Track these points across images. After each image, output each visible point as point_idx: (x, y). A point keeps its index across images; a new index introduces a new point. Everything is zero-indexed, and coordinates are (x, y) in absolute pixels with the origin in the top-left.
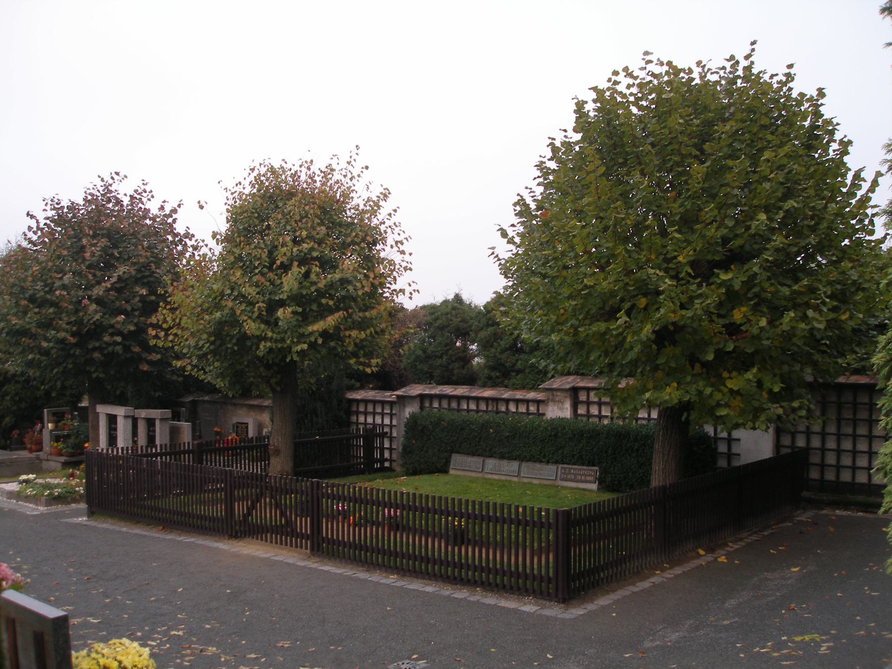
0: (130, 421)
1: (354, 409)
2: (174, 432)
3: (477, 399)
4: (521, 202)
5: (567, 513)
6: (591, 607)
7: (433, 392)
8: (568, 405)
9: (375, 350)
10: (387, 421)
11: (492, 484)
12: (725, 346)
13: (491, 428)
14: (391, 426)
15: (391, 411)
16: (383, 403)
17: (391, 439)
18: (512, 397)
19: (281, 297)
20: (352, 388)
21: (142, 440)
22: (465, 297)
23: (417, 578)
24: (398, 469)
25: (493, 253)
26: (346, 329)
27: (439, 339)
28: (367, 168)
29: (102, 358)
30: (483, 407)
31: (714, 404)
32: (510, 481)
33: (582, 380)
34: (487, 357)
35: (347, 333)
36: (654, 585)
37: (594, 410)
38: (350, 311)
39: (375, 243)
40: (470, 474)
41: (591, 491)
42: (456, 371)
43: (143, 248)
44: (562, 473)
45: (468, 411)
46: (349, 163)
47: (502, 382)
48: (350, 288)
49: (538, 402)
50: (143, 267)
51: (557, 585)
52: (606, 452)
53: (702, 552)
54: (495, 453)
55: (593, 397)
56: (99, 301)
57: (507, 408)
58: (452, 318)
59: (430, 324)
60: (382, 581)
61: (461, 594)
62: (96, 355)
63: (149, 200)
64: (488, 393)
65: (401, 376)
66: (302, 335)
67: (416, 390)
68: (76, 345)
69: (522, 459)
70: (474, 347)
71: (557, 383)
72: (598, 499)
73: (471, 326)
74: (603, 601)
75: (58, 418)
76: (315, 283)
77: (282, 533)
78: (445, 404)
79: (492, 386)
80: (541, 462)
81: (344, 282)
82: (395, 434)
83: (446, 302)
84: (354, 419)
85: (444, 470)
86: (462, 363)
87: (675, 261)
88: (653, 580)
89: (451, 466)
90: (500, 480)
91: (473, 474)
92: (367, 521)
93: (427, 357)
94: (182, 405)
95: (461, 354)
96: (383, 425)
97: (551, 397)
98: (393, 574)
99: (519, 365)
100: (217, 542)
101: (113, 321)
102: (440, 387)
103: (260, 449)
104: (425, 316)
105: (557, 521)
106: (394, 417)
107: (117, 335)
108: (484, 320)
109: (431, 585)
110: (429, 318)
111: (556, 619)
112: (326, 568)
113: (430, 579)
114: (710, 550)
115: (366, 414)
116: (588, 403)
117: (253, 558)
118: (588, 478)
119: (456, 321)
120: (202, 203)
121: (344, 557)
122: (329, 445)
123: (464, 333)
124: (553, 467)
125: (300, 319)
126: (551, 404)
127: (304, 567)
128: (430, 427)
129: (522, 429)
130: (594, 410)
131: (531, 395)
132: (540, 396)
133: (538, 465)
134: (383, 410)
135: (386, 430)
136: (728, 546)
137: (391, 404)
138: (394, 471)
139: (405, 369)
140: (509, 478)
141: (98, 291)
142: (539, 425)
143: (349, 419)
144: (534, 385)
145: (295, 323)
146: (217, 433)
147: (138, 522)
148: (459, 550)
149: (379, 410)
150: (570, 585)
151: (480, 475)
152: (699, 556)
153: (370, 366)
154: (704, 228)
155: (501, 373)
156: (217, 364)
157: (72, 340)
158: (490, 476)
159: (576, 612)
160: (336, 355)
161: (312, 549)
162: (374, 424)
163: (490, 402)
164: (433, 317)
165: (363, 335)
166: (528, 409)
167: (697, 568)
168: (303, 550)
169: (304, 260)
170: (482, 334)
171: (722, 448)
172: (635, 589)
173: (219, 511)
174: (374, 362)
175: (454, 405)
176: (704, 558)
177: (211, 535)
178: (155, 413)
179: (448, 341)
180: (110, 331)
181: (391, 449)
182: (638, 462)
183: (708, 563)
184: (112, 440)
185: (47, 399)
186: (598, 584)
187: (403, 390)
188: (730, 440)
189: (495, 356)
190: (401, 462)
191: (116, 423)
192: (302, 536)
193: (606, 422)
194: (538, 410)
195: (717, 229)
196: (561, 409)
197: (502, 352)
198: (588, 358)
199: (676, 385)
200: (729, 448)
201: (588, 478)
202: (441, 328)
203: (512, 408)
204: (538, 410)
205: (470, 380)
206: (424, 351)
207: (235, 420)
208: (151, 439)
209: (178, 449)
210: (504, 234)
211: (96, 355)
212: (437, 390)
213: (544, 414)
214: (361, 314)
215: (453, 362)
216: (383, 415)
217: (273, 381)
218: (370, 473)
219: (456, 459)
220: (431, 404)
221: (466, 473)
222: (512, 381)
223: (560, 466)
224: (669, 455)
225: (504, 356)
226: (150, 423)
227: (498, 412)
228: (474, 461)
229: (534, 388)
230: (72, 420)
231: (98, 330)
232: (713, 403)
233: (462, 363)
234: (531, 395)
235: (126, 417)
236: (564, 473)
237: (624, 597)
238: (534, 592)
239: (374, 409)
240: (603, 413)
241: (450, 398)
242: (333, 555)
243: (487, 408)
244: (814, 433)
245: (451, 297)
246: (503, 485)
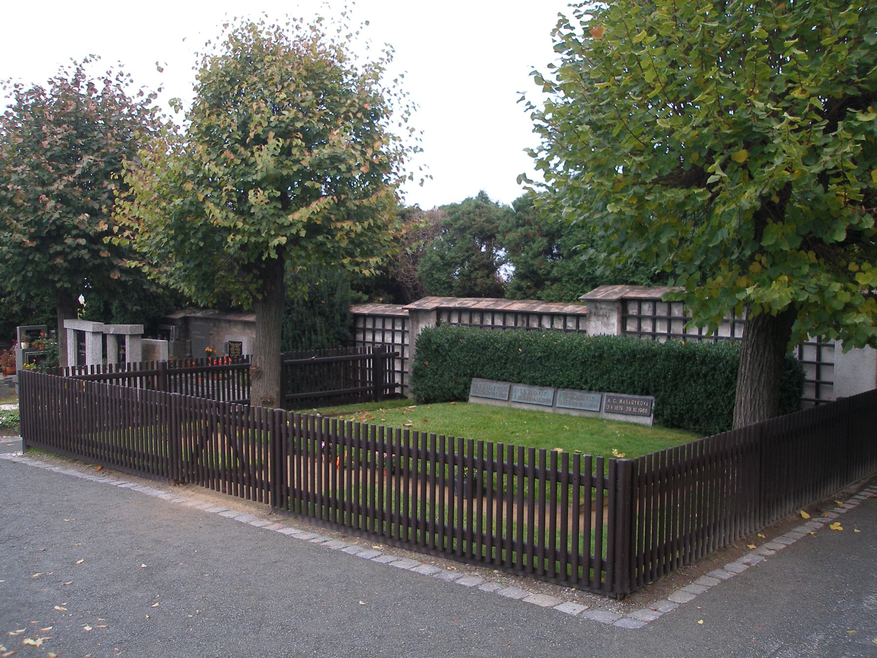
0: (100, 338)
1: (361, 325)
2: (148, 351)
3: (505, 313)
4: (563, 22)
5: (632, 466)
6: (664, 607)
7: (451, 305)
8: (614, 320)
9: (376, 248)
10: (398, 340)
11: (519, 416)
12: (861, 221)
13: (520, 346)
14: (403, 346)
15: (403, 328)
16: (394, 318)
17: (403, 361)
18: (545, 311)
19: (255, 177)
20: (358, 302)
21: (112, 359)
22: (493, 198)
23: (410, 549)
24: (410, 396)
25: (523, 98)
26: (338, 220)
27: (459, 243)
28: (367, 23)
29: (66, 265)
30: (511, 322)
31: (840, 307)
32: (543, 412)
33: (632, 290)
34: (516, 263)
35: (339, 225)
36: (751, 569)
37: (647, 327)
38: (343, 197)
39: (377, 117)
40: (493, 403)
41: (644, 426)
42: (479, 281)
43: (113, 136)
44: (607, 403)
45: (493, 327)
46: (343, 14)
47: (534, 294)
48: (343, 167)
49: (578, 317)
50: (115, 159)
51: (614, 572)
52: (664, 378)
53: (805, 515)
54: (525, 377)
55: (647, 310)
56: (62, 198)
57: (540, 324)
58: (475, 223)
59: (448, 226)
60: (361, 555)
61: (471, 579)
62: (59, 261)
63: (127, 85)
64: (517, 306)
65: (415, 288)
66: (282, 227)
67: (431, 303)
68: (37, 249)
69: (557, 385)
70: (502, 253)
71: (601, 293)
72: (676, 445)
73: (497, 227)
74: (682, 596)
75: (33, 335)
76: (297, 162)
77: (236, 479)
78: (465, 319)
79: (523, 299)
80: (582, 389)
81: (335, 159)
82: (407, 355)
83: (468, 200)
84: (360, 337)
85: (462, 398)
86: (486, 272)
87: (787, 97)
88: (746, 559)
89: (471, 393)
90: (531, 411)
91: (498, 403)
92: (359, 464)
93: (445, 265)
94: (172, 322)
95: (485, 261)
96: (393, 344)
97: (593, 310)
98: (378, 542)
99: (555, 273)
100: (159, 488)
101: (76, 222)
102: (461, 300)
103: (239, 367)
104: (444, 216)
105: (616, 478)
106: (406, 335)
107: (82, 237)
108: (513, 220)
109: (428, 563)
110: (448, 219)
111: (612, 629)
112: (288, 531)
113: (428, 554)
114: (816, 512)
115: (374, 331)
116: (640, 318)
117: (197, 514)
118: (641, 410)
119: (480, 221)
120: (162, 65)
121: (314, 516)
122: (327, 364)
123: (488, 237)
124: (596, 396)
125: (280, 206)
126: (593, 318)
127: (260, 529)
128: (447, 345)
129: (558, 348)
130: (647, 327)
131: (570, 308)
132: (580, 309)
133: (577, 393)
134: (393, 327)
135: (398, 350)
136: (837, 506)
137: (403, 319)
138: (406, 398)
139: (420, 279)
140: (541, 409)
141: (58, 186)
142: (580, 344)
143: (355, 337)
144: (572, 297)
145: (272, 211)
146: (209, 354)
147: (75, 460)
148: (468, 513)
149: (389, 327)
150: (630, 570)
152: (801, 521)
153: (367, 265)
154: (837, 43)
155: (532, 283)
156: (179, 264)
157: (29, 243)
158: (518, 406)
159: (642, 616)
160: (326, 253)
161: (274, 504)
162: (383, 343)
163: (519, 317)
164: (453, 217)
165: (359, 228)
166: (565, 325)
167: (803, 539)
168: (263, 504)
169: (285, 133)
170: (510, 236)
171: (810, 375)
172: (726, 576)
173: (164, 449)
174: (373, 261)
175: (476, 320)
176: (811, 526)
177: (155, 480)
178: (125, 329)
179: (470, 245)
180: (74, 232)
181: (402, 373)
182: (705, 390)
183: (818, 531)
184: (81, 359)
185: (26, 314)
186: (672, 568)
187: (417, 303)
188: (819, 365)
189: (526, 262)
190: (412, 388)
191: (84, 341)
192: (261, 485)
193: (663, 341)
194: (578, 326)
195: (850, 50)
196: (606, 325)
197: (535, 256)
198: (656, 242)
199: (786, 278)
200: (818, 375)
201: (641, 410)
202: (463, 230)
203: (546, 324)
204: (578, 326)
205: (497, 291)
206: (442, 258)
207: (228, 338)
208: (121, 358)
209: (150, 369)
210: (539, 80)
211: (59, 261)
212: (457, 303)
213: (585, 332)
214: (357, 202)
215: (476, 269)
216: (393, 332)
217: (253, 287)
218: (376, 401)
219: (478, 385)
220: (449, 320)
221: (489, 402)
222: (546, 292)
223: (606, 394)
224: (759, 380)
225: (536, 262)
226: (120, 340)
227: (528, 329)
228: (499, 388)
229: (573, 300)
230: (47, 339)
231: (59, 232)
232: (838, 305)
233: (486, 272)
234: (570, 308)
235: (94, 333)
237: (711, 589)
238: (578, 580)
239: (384, 325)
240: (658, 330)
241: (472, 312)
242: (300, 513)
243: (516, 324)
245: (474, 195)
246: (534, 417)
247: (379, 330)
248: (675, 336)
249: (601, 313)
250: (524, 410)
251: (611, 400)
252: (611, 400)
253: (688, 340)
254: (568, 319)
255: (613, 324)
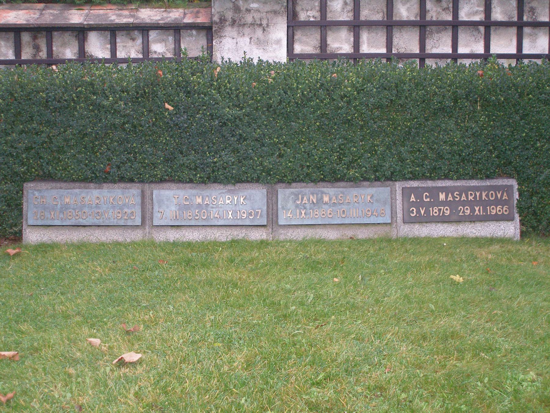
41: (502, 241)
57: (82, 51)
118: (493, 211)
126: (229, 31)
151: (137, 236)
163: (26, 37)
196: (261, 43)
201: (493, 211)
223: (399, 186)
236: (419, 204)
243: (18, 52)
244: (178, 42)
247: (474, 25)
248: (401, 57)
249: (249, 19)
250: (189, 245)
251: (419, 196)
252: (419, 196)
253: (429, 62)
254: (153, 35)
255: (278, 42)
